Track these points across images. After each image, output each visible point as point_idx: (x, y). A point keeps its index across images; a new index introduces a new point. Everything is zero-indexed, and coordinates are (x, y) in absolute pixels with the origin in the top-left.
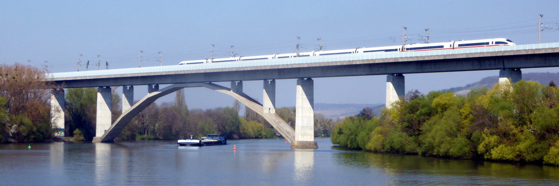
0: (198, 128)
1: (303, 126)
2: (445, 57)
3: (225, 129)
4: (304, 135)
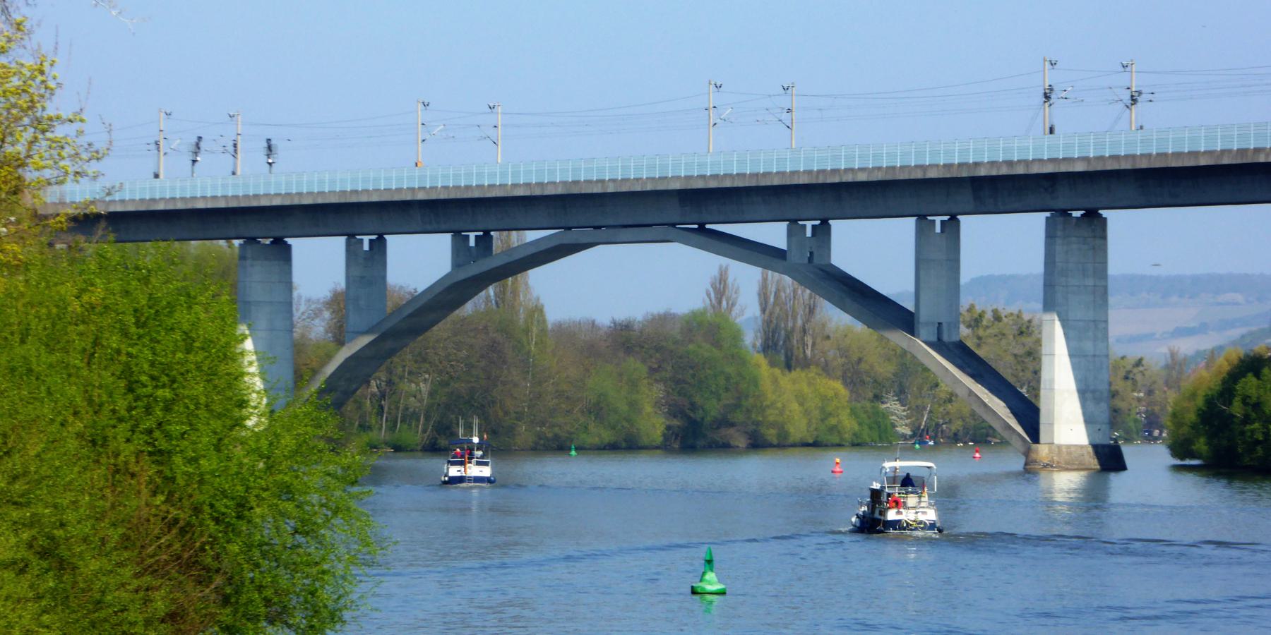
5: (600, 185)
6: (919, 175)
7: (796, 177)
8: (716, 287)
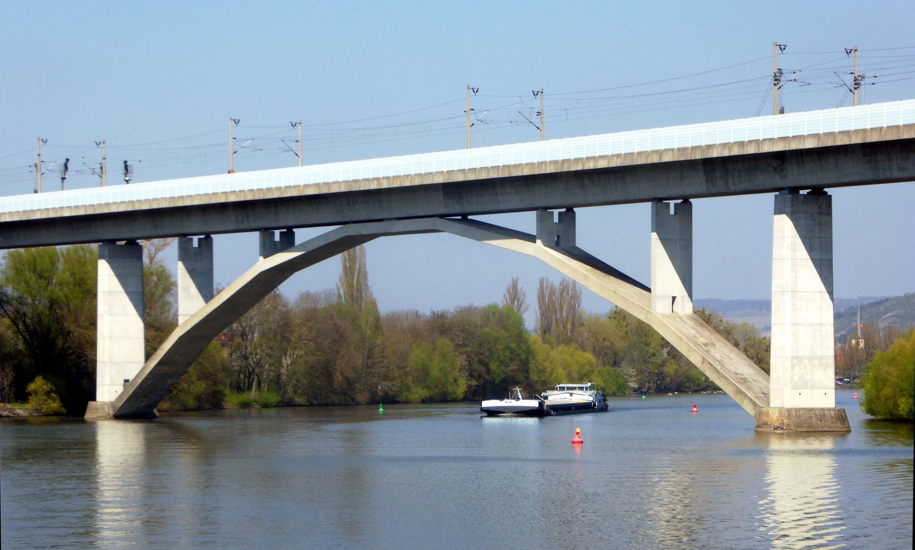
0: (408, 369)
1: (797, 357)
3: (488, 370)
4: (799, 386)
5: (375, 182)
6: (655, 160)
7: (543, 167)
8: (510, 292)
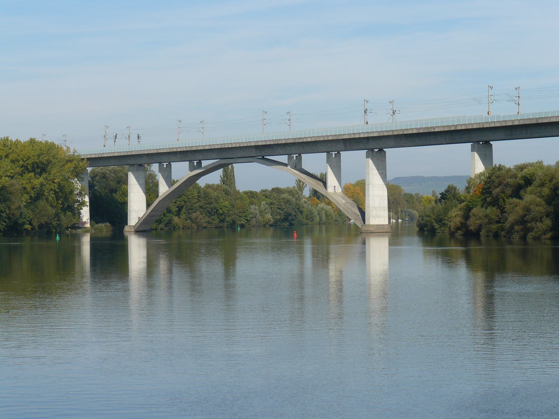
2: (456, 127)
